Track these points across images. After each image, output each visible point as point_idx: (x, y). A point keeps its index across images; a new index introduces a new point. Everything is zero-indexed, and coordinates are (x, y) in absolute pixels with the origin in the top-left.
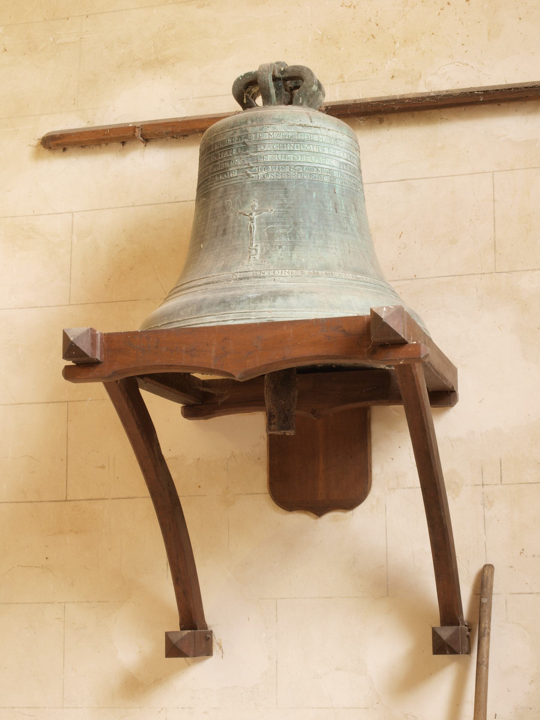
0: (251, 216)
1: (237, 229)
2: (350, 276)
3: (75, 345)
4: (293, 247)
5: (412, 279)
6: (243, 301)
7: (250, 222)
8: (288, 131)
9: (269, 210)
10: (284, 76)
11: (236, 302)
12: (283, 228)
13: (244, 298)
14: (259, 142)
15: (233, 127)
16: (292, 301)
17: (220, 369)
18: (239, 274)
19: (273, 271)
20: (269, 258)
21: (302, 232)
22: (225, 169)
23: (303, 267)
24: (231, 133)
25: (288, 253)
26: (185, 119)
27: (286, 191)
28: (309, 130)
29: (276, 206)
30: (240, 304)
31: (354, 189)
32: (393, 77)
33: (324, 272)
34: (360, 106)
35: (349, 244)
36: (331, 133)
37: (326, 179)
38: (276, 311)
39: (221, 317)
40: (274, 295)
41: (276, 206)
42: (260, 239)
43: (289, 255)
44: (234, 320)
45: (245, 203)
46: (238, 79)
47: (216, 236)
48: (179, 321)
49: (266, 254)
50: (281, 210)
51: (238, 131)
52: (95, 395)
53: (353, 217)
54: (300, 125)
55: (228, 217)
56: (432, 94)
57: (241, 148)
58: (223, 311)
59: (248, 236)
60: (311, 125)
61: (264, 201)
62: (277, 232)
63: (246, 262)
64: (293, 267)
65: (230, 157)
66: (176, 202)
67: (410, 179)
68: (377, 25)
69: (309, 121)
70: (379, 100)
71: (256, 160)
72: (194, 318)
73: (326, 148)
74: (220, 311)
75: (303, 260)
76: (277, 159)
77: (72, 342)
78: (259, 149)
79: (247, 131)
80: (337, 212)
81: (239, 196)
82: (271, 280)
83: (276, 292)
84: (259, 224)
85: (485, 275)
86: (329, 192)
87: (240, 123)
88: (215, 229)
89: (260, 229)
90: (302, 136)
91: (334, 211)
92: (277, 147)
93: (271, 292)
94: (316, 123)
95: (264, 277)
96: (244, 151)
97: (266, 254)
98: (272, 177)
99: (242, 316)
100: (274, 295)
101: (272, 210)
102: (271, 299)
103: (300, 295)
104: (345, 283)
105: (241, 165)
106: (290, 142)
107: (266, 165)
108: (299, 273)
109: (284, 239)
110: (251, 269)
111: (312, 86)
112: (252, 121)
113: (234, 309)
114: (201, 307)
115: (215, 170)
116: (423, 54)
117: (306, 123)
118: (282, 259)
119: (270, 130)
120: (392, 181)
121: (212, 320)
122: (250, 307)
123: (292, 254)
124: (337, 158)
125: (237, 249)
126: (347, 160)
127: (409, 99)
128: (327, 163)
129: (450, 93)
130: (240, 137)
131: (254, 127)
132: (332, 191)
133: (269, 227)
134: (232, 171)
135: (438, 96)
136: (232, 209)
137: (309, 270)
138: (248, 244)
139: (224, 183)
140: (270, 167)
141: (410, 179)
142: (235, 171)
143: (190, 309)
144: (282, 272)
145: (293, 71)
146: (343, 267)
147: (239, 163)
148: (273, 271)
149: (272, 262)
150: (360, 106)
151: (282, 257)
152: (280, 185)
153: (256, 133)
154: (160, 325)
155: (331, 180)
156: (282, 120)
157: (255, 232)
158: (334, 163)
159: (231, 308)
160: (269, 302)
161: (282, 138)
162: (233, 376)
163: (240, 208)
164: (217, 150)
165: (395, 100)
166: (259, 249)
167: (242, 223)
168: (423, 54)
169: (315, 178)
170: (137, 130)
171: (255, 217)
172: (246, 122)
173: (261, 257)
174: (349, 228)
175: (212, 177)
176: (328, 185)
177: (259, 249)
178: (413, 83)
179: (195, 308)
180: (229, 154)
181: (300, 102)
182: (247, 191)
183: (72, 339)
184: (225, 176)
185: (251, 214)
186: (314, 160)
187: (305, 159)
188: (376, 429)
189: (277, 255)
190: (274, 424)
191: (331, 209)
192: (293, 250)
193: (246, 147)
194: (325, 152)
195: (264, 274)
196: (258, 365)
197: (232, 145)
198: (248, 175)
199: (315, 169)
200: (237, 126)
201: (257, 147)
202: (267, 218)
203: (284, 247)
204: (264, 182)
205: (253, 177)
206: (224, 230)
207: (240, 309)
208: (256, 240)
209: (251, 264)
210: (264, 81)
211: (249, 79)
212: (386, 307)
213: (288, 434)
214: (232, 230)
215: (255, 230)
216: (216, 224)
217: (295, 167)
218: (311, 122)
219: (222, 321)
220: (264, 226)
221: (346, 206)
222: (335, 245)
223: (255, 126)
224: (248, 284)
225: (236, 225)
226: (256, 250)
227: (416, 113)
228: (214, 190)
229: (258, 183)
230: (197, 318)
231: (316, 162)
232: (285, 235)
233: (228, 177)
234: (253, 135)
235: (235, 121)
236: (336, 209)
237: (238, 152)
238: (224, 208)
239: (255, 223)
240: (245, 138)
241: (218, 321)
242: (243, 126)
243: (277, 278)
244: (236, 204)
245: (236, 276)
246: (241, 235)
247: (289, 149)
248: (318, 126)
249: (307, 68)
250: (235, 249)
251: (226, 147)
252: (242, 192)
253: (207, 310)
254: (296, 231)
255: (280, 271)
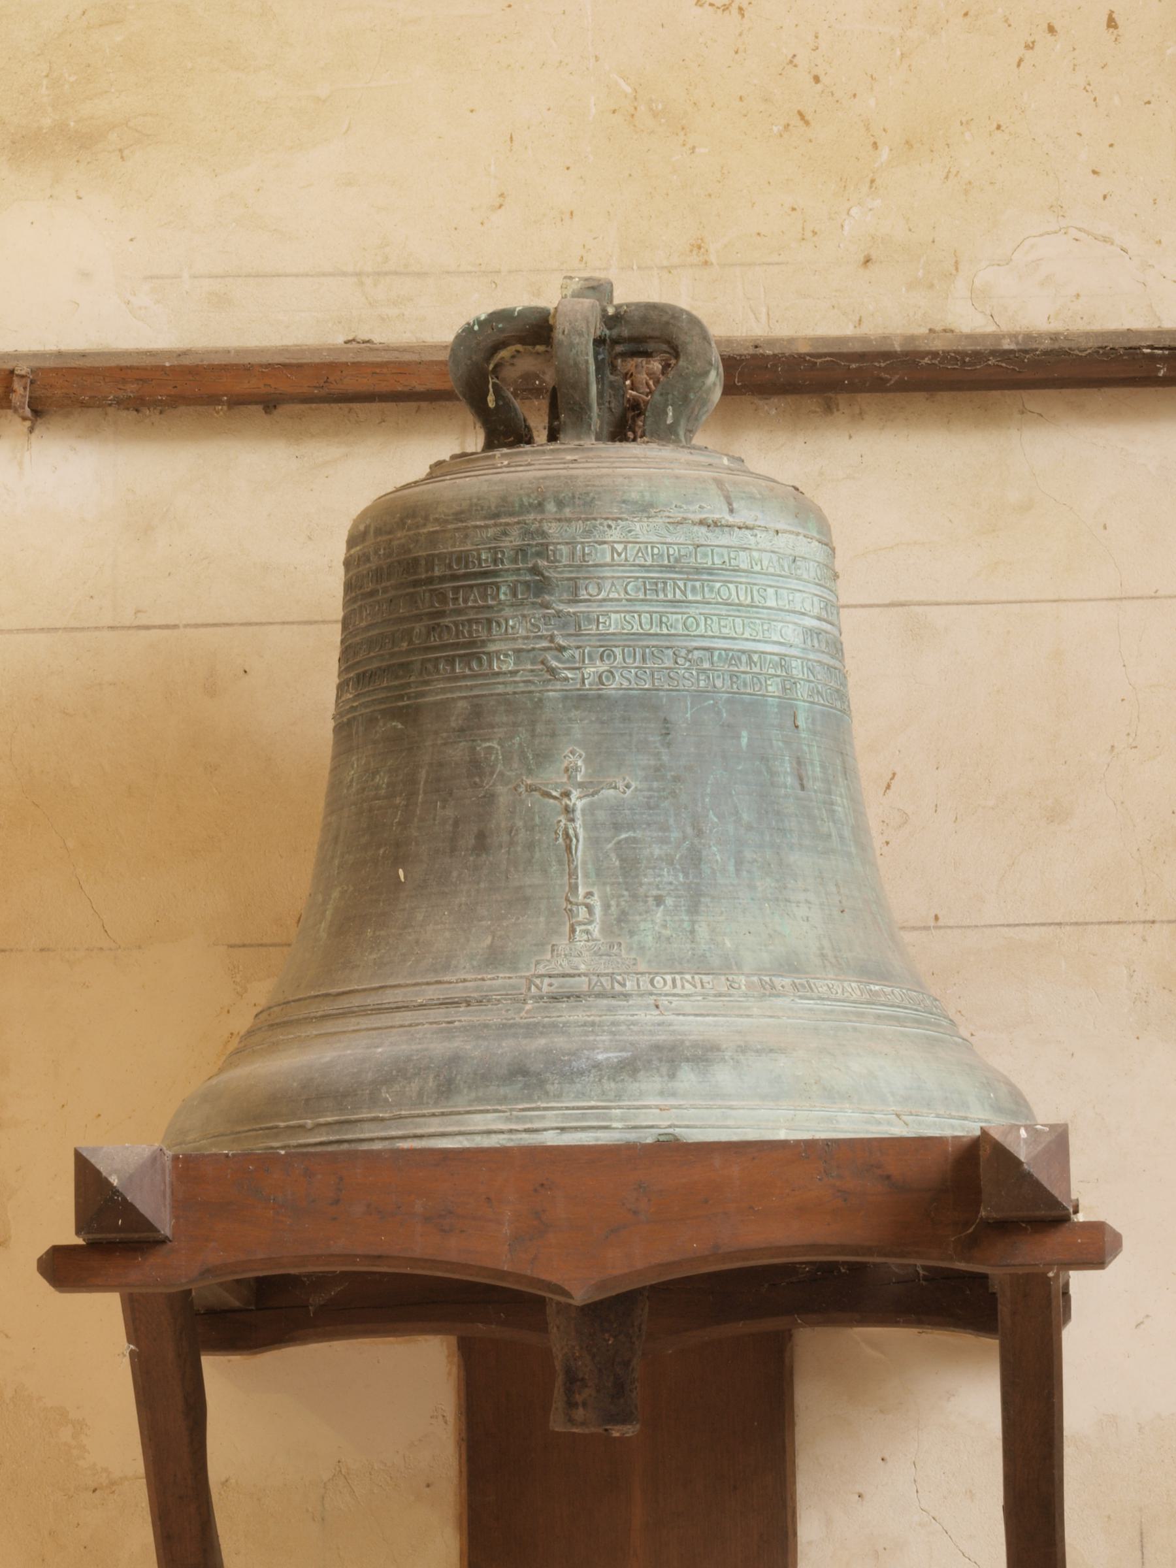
0: (565, 801)
1: (522, 836)
2: (853, 988)
3: (125, 1199)
4: (694, 901)
5: (926, 928)
6: (581, 1073)
7: (562, 818)
8: (669, 540)
9: (621, 785)
10: (615, 332)
11: (563, 1075)
12: (664, 841)
13: (583, 1064)
14: (583, 571)
15: (497, 516)
16: (723, 1076)
17: (529, 1273)
18: (547, 981)
19: (647, 978)
20: (632, 933)
21: (715, 854)
22: (472, 644)
23: (728, 966)
24: (491, 532)
25: (682, 921)
26: (186, 361)
27: (666, 728)
28: (724, 540)
29: (640, 773)
30: (572, 1082)
31: (838, 704)
32: (867, 261)
33: (787, 981)
34: (775, 366)
35: (837, 885)
36: (781, 542)
37: (773, 688)
38: (679, 1107)
39: (519, 1120)
40: (670, 1056)
41: (640, 773)
42: (597, 875)
43: (686, 925)
44: (563, 1129)
45: (544, 757)
46: (468, 330)
47: (453, 850)
48: (383, 1120)
49: (619, 924)
50: (655, 785)
51: (515, 532)
52: (98, 1321)
53: (841, 796)
54: (702, 523)
55: (491, 798)
56: (1007, 345)
57: (527, 584)
58: (522, 1100)
59: (560, 862)
60: (730, 519)
61: (603, 755)
62: (647, 852)
63: (563, 943)
64: (701, 966)
65: (490, 607)
66: (139, 627)
67: (919, 604)
68: (817, 79)
69: (725, 508)
70: (835, 350)
71: (574, 626)
72: (434, 1115)
73: (771, 591)
74: (516, 1100)
75: (728, 944)
76: (636, 629)
77: (115, 1191)
78: (583, 595)
79: (543, 534)
80: (803, 787)
81: (523, 735)
82: (647, 1007)
83: (673, 1048)
84: (593, 826)
85: (1157, 926)
86: (781, 727)
87: (522, 505)
88: (449, 828)
89: (594, 843)
90: (705, 555)
91: (797, 786)
92: (638, 589)
93: (657, 1048)
94: (744, 515)
95: (626, 996)
96: (536, 595)
97: (619, 921)
98: (625, 684)
99: (583, 1117)
100: (670, 1056)
101: (628, 786)
102: (664, 1070)
103: (742, 1057)
104: (846, 1013)
105: (527, 638)
106: (678, 573)
107: (605, 647)
108: (722, 984)
109: (667, 875)
110: (583, 968)
111: (706, 374)
112: (560, 504)
113: (558, 1096)
114: (450, 1081)
115: (434, 641)
116: (966, 192)
117: (716, 516)
118: (668, 939)
119: (614, 535)
120: (863, 606)
121: (494, 1127)
122: (603, 1093)
123: (693, 922)
124: (796, 618)
125: (527, 900)
126: (819, 619)
127: (935, 354)
128: (775, 638)
129: (1066, 345)
130: (521, 552)
131: (565, 524)
132: (789, 723)
133: (623, 836)
134: (498, 653)
135: (1026, 352)
136: (501, 774)
137: (748, 975)
138: (561, 886)
139: (471, 688)
140: (618, 651)
141: (919, 604)
142: (506, 655)
143: (415, 1086)
144: (674, 981)
145: (645, 320)
146: (833, 960)
147: (522, 632)
148: (647, 978)
149: (642, 948)
150: (775, 366)
151: (668, 932)
152: (647, 706)
153: (571, 543)
154: (309, 1123)
155: (784, 689)
156: (651, 505)
157: (581, 851)
158: (792, 634)
159: (547, 1093)
160: (657, 1079)
161: (649, 562)
162: (567, 1294)
163: (530, 772)
164: (442, 579)
165: (887, 355)
166: (596, 902)
167: (537, 820)
168: (966, 192)
169: (745, 685)
170: (17, 385)
171: (580, 804)
172: (540, 504)
173: (607, 930)
174: (834, 833)
175: (424, 661)
176: (780, 706)
177: (596, 902)
178: (931, 286)
179: (431, 1083)
180: (484, 597)
181: (669, 421)
182: (548, 722)
183: (114, 1180)
184: (474, 665)
185: (567, 794)
186: (739, 630)
187: (715, 627)
188: (811, 1401)
189: (653, 925)
190: (584, 1404)
191: (789, 780)
192: (697, 912)
193: (540, 585)
194: (769, 604)
195: (623, 985)
196: (640, 1265)
197: (494, 573)
198: (552, 671)
199: (744, 658)
200: (512, 514)
201: (576, 588)
202: (615, 809)
203: (669, 901)
204: (600, 697)
205: (566, 679)
206: (481, 836)
207: (577, 1098)
208: (586, 875)
209: (580, 952)
210: (576, 364)
211: (502, 330)
212: (1026, 1127)
213: (616, 1434)
214: (505, 838)
215: (580, 846)
216: (450, 812)
217: (689, 651)
218: (731, 511)
219: (526, 1131)
220: (609, 834)
221: (823, 767)
222: (805, 890)
223: (569, 520)
224: (579, 1016)
225: (520, 824)
226: (588, 906)
227: (946, 396)
228: (435, 703)
229: (583, 698)
230: (443, 1114)
231: (746, 635)
232: (671, 862)
233: (485, 669)
234: (564, 549)
235: (504, 499)
236: (801, 779)
237: (515, 595)
238: (476, 767)
239: (578, 823)
240: (539, 554)
241: (511, 1131)
242: (532, 516)
243: (664, 1001)
244: (516, 758)
245: (539, 989)
246: (537, 855)
247: (670, 596)
248: (750, 523)
249: (688, 313)
250: (522, 900)
251: (475, 575)
252: (533, 723)
253: (473, 1095)
254: (700, 852)
255: (668, 978)
